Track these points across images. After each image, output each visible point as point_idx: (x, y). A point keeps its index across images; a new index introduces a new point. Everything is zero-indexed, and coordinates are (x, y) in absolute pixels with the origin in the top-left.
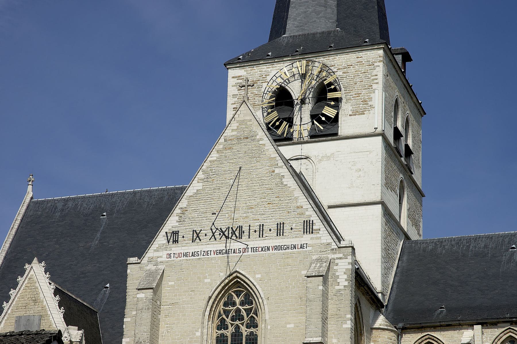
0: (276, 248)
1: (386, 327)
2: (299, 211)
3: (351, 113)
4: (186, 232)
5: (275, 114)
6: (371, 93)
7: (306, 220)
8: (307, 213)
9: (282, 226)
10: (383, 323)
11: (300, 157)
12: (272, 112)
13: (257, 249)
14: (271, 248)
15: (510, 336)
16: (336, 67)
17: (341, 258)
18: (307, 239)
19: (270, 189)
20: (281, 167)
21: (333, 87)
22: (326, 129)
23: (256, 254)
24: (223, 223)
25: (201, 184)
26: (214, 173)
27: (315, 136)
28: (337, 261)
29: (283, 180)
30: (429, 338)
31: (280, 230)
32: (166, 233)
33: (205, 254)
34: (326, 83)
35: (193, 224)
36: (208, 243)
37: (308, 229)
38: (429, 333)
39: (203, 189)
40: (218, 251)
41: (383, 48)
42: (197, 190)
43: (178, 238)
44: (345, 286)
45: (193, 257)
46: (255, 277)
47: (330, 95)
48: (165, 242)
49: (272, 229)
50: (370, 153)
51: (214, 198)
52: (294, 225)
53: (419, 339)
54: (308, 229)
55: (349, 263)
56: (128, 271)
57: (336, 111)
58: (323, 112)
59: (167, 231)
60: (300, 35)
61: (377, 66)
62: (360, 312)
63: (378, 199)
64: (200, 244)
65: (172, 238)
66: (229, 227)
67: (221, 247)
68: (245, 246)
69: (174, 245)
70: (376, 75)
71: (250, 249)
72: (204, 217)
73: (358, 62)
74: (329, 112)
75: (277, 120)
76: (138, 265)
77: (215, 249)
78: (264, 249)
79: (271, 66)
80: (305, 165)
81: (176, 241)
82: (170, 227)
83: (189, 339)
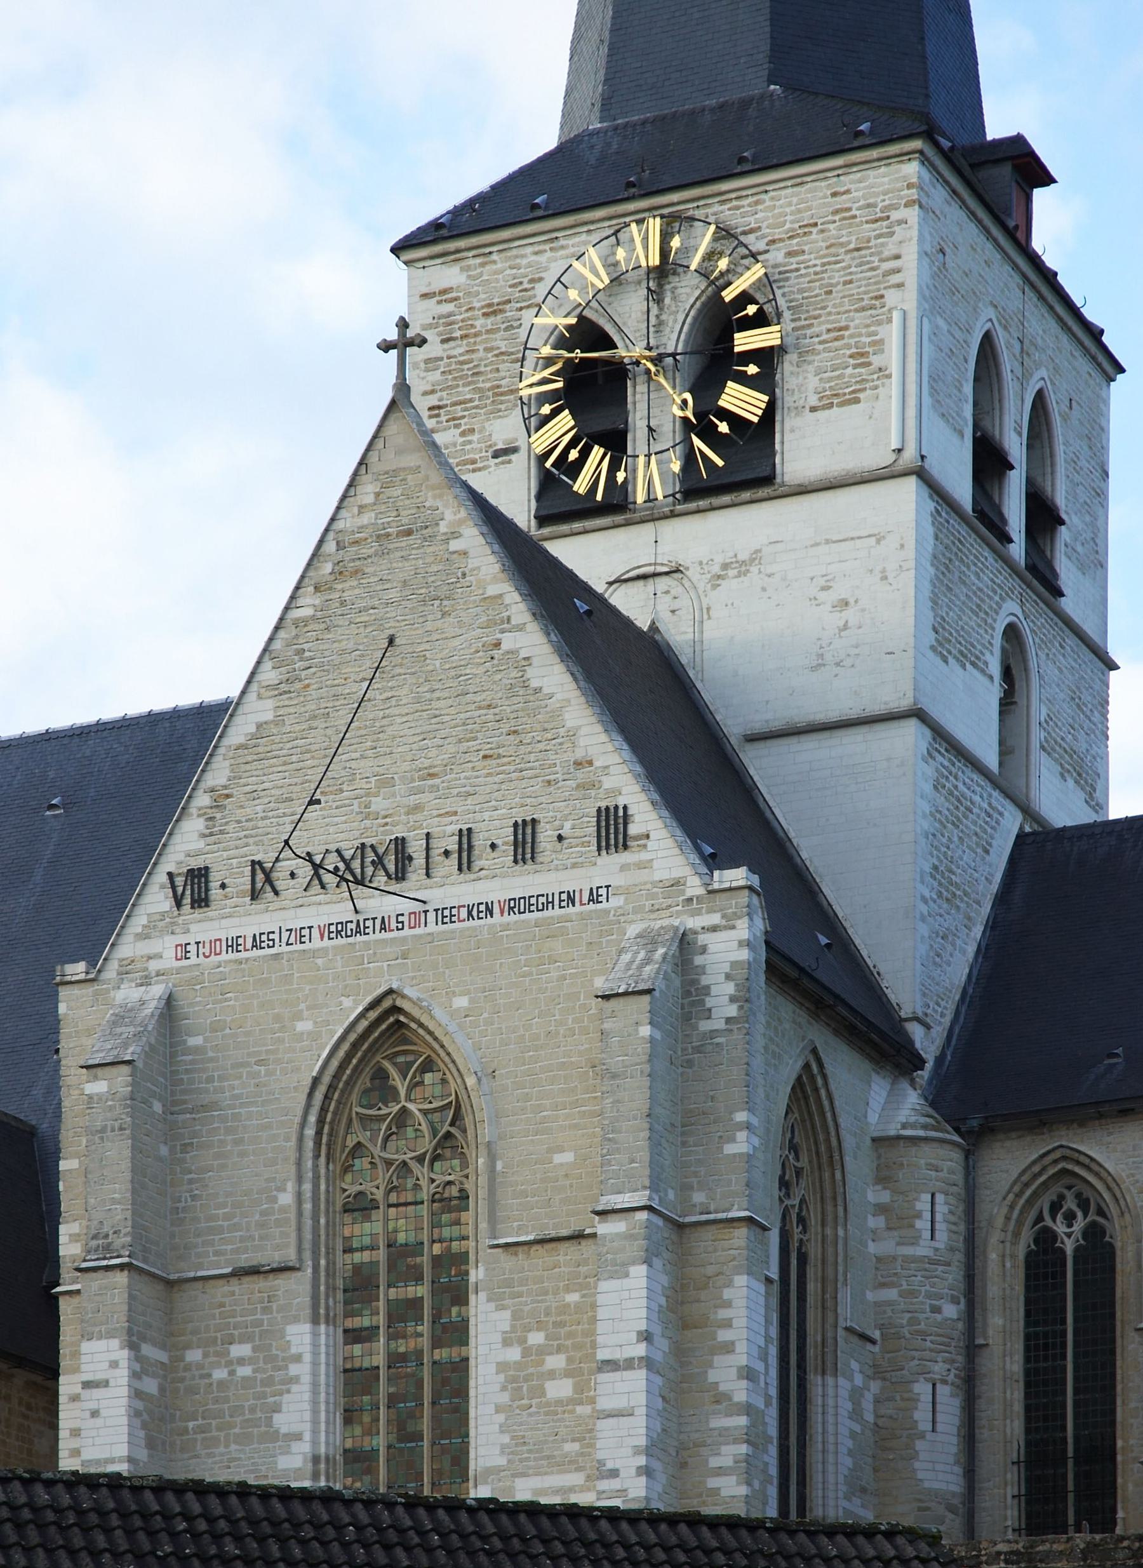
0: (513, 906)
1: (921, 1133)
2: (581, 775)
3: (813, 401)
4: (230, 871)
5: (565, 421)
6: (879, 323)
7: (603, 805)
8: (608, 783)
9: (529, 830)
10: (913, 1119)
11: (651, 569)
12: (555, 413)
13: (454, 911)
14: (496, 910)
15: (1064, 1171)
16: (763, 237)
17: (714, 929)
18: (608, 869)
19: (489, 706)
20: (520, 628)
21: (751, 309)
22: (737, 464)
23: (453, 931)
24: (333, 831)
25: (269, 704)
26: (307, 664)
27: (698, 490)
28: (702, 939)
29: (530, 672)
30: (1064, 1158)
31: (525, 843)
32: (170, 875)
33: (292, 940)
34: (729, 295)
35: (251, 840)
36: (300, 901)
37: (612, 836)
38: (1064, 1143)
39: (278, 721)
40: (333, 928)
41: (921, 152)
42: (259, 726)
43: (207, 890)
44: (728, 1020)
45: (256, 953)
46: (448, 1010)
47: (744, 341)
48: (167, 904)
49: (498, 842)
50: (878, 541)
51: (313, 747)
52: (568, 825)
53: (1034, 1163)
54: (612, 836)
55: (741, 944)
56: (62, 1008)
57: (766, 398)
58: (721, 403)
59: (171, 868)
60: (644, 123)
61: (900, 222)
62: (823, 1092)
63: (906, 703)
64: (276, 905)
65: (188, 892)
66: (363, 844)
67: (342, 912)
68: (417, 907)
69: (198, 914)
70: (897, 257)
71: (431, 916)
72: (285, 815)
73: (836, 212)
74: (741, 400)
75: (572, 444)
76: (89, 990)
77: (324, 921)
78: (475, 913)
79: (547, 247)
80: (668, 598)
81: (201, 901)
82: (181, 857)
83: (257, 1217)
